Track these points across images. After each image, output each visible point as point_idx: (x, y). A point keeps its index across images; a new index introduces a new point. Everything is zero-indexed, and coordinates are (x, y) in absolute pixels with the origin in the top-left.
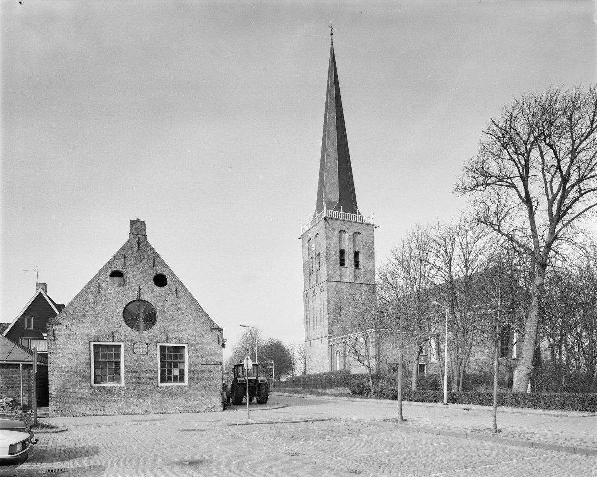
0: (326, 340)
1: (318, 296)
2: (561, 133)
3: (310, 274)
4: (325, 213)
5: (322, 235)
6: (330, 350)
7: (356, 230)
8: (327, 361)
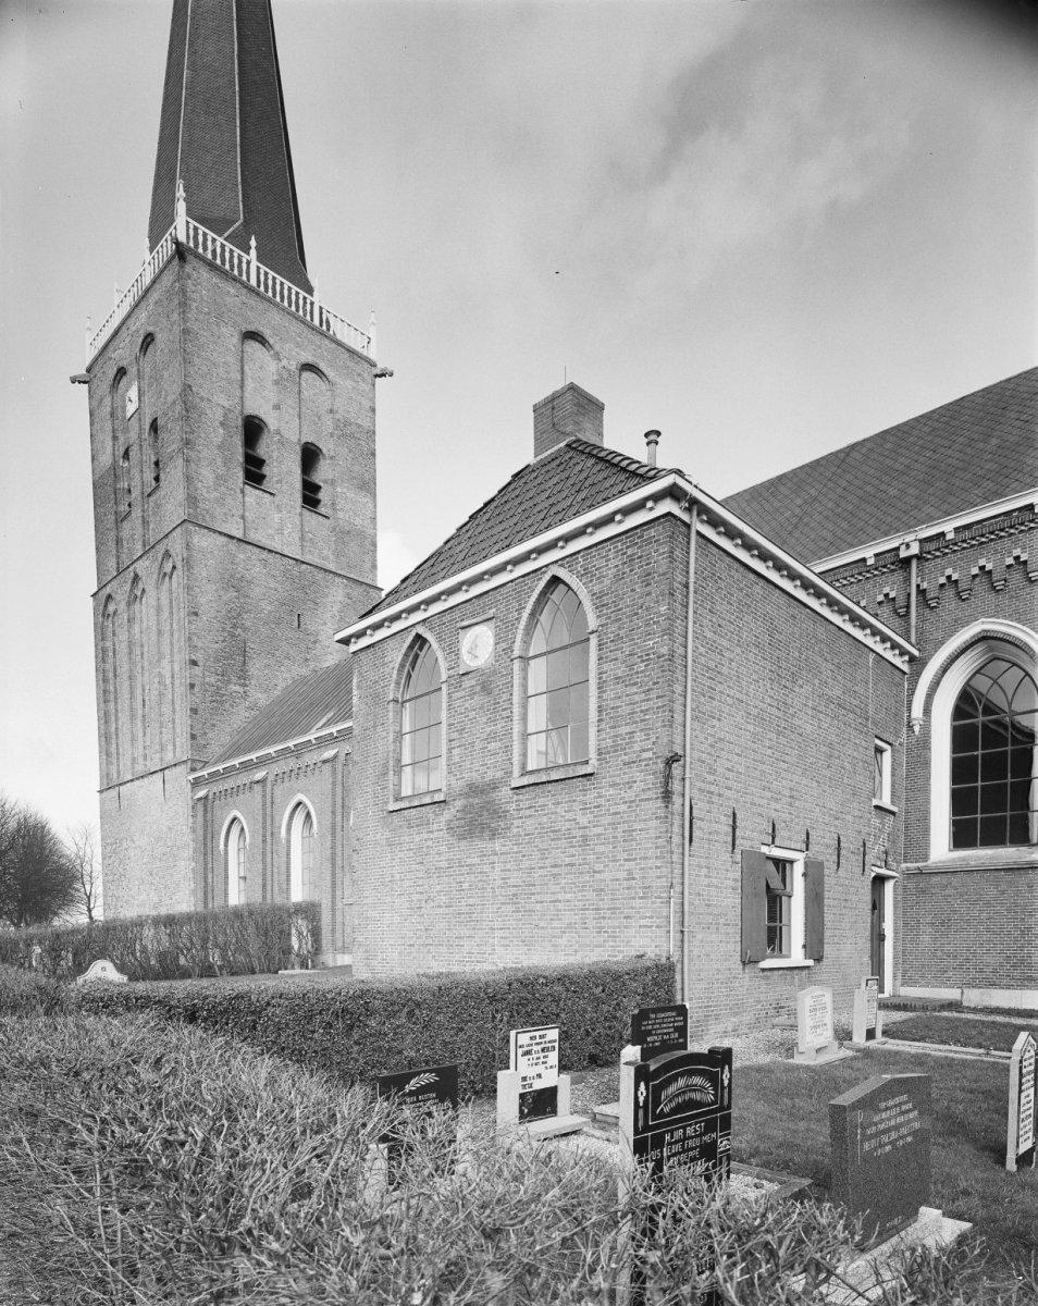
0: (181, 778)
1: (150, 599)
3: (121, 519)
6: (200, 818)
7: (310, 359)
8: (185, 867)
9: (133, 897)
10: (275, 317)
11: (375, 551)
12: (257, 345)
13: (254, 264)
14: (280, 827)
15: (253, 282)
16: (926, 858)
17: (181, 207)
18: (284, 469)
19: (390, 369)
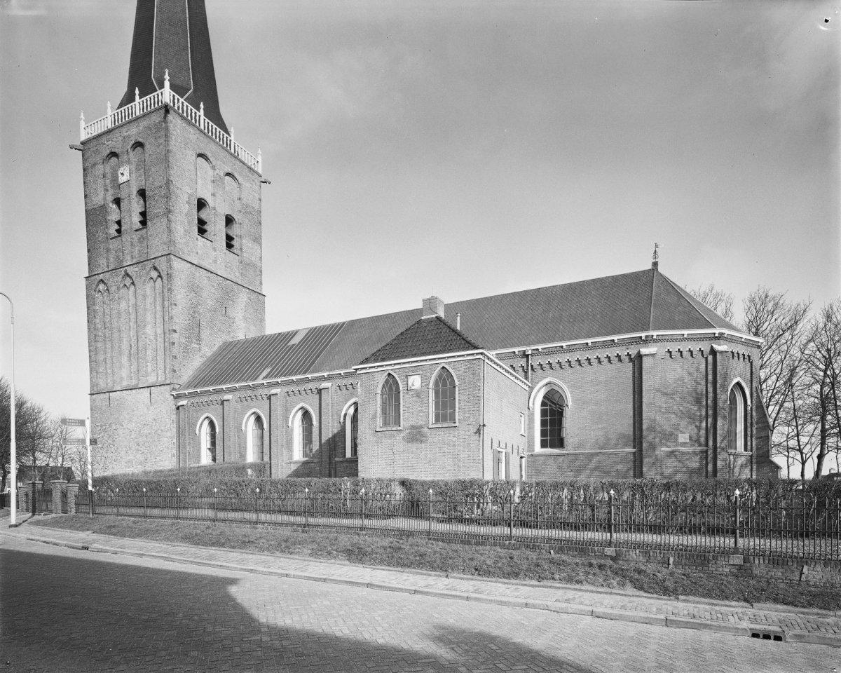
9: (121, 457)
10: (213, 147)
11: (261, 275)
12: (203, 160)
13: (203, 117)
15: (202, 127)
16: (533, 451)
17: (167, 84)
18: (217, 228)
19: (269, 180)
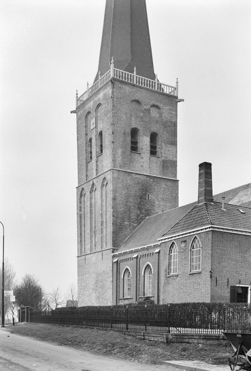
2: (121, 93)
4: (111, 72)
5: (106, 107)
14: (142, 272)
